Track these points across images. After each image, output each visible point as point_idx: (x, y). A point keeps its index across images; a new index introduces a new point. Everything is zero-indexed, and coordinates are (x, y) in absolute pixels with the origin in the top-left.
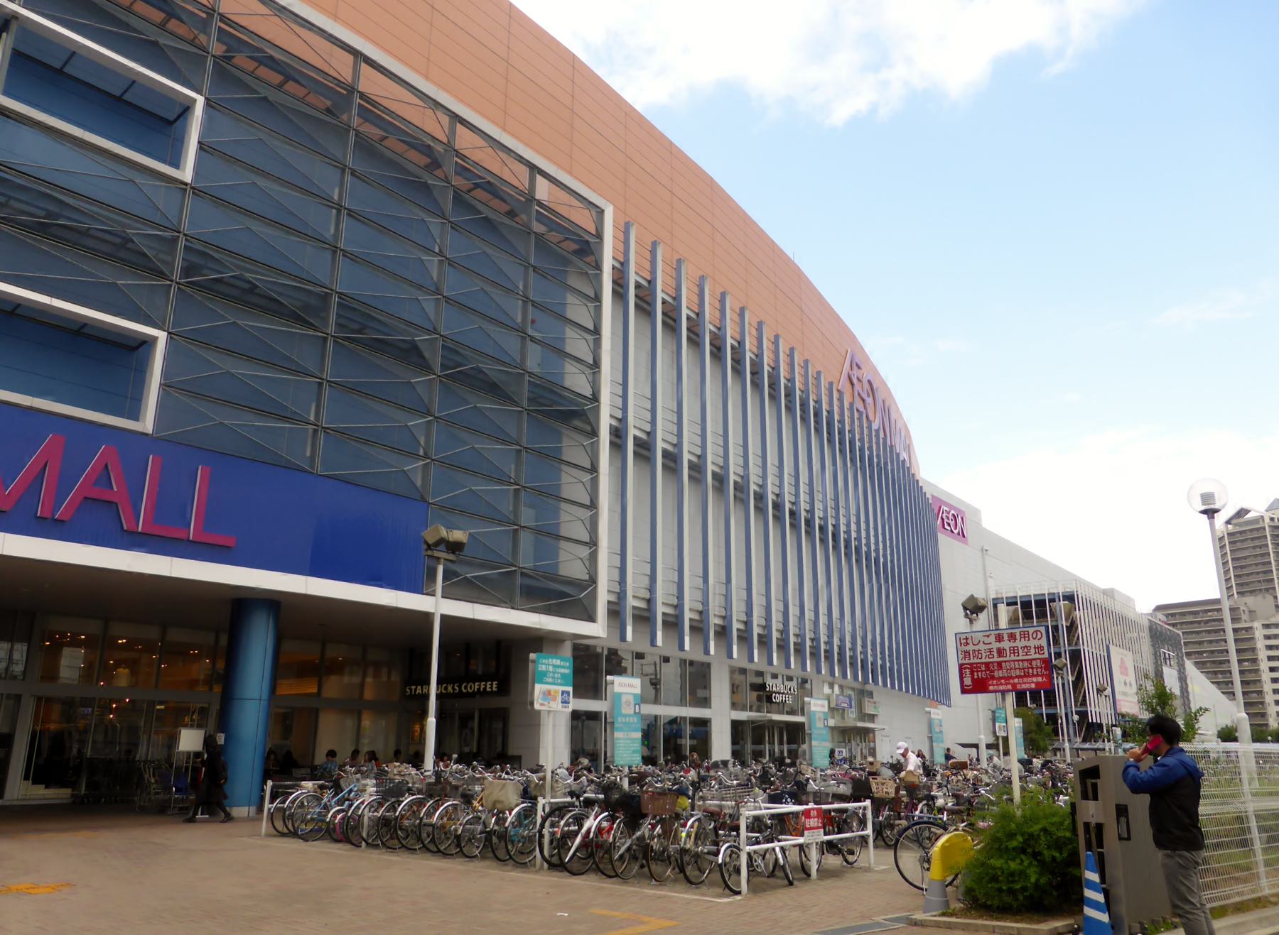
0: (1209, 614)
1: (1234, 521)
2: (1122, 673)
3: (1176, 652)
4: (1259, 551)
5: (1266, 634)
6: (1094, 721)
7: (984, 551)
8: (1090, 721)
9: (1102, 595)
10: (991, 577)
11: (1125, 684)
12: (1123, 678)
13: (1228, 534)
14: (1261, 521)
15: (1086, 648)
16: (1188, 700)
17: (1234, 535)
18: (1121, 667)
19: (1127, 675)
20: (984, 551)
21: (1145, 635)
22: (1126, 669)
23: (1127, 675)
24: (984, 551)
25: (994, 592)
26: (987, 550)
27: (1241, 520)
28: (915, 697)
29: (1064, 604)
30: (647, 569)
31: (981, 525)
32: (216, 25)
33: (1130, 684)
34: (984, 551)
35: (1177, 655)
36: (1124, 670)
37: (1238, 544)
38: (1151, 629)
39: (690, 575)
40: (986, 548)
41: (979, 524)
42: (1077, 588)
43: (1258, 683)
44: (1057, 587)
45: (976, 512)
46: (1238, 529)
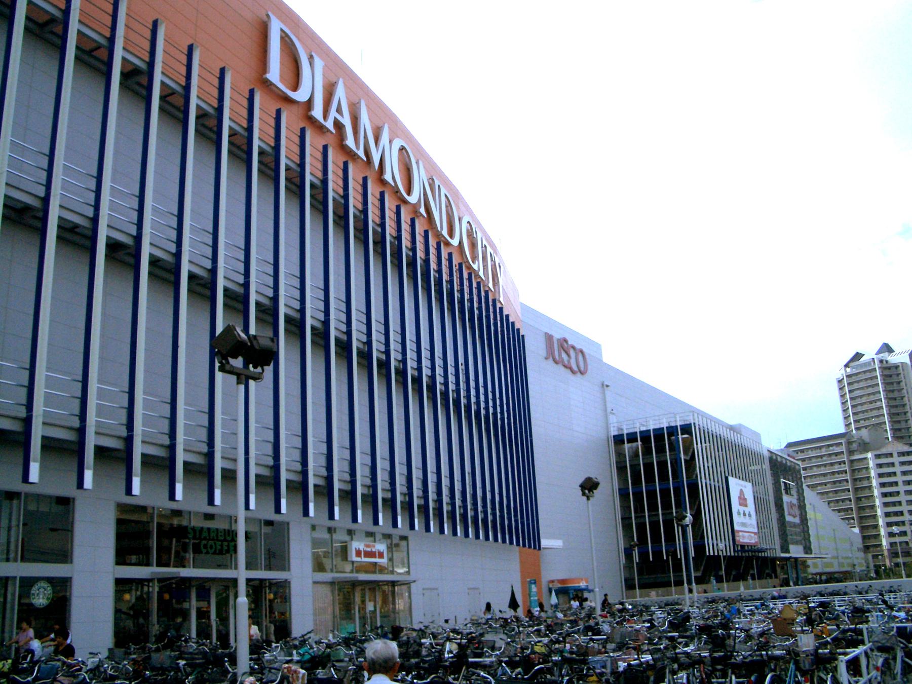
0: (831, 448)
1: (852, 364)
2: (741, 504)
3: (795, 482)
4: (870, 390)
5: (884, 491)
6: (712, 554)
7: (605, 386)
8: (708, 554)
9: (728, 430)
10: (613, 414)
11: (744, 514)
12: (742, 509)
13: (847, 376)
14: (872, 363)
15: (703, 482)
16: (808, 527)
17: (855, 399)
18: (740, 498)
19: (746, 506)
20: (604, 386)
21: (766, 466)
22: (745, 499)
23: (746, 506)
24: (605, 386)
25: (616, 429)
26: (607, 386)
27: (857, 363)
28: (532, 550)
29: (683, 439)
30: (298, 442)
31: (602, 361)
32: (832, 594)
33: (750, 515)
34: (604, 386)
35: (797, 484)
36: (743, 501)
37: (861, 422)
38: (771, 459)
39: (338, 447)
40: (606, 383)
41: (600, 361)
42: (694, 419)
43: (871, 498)
44: (676, 421)
45: (598, 347)
46: (855, 371)
